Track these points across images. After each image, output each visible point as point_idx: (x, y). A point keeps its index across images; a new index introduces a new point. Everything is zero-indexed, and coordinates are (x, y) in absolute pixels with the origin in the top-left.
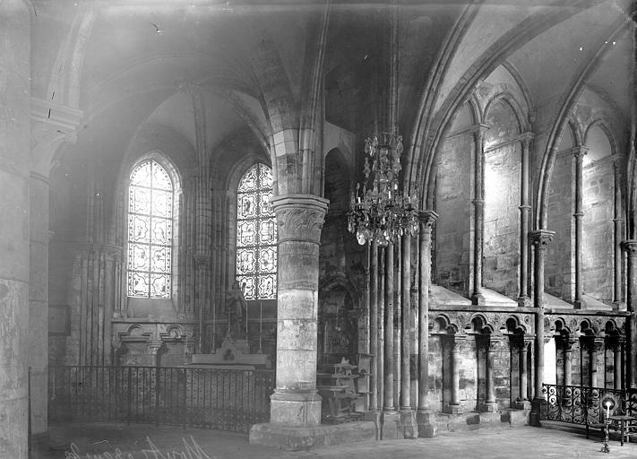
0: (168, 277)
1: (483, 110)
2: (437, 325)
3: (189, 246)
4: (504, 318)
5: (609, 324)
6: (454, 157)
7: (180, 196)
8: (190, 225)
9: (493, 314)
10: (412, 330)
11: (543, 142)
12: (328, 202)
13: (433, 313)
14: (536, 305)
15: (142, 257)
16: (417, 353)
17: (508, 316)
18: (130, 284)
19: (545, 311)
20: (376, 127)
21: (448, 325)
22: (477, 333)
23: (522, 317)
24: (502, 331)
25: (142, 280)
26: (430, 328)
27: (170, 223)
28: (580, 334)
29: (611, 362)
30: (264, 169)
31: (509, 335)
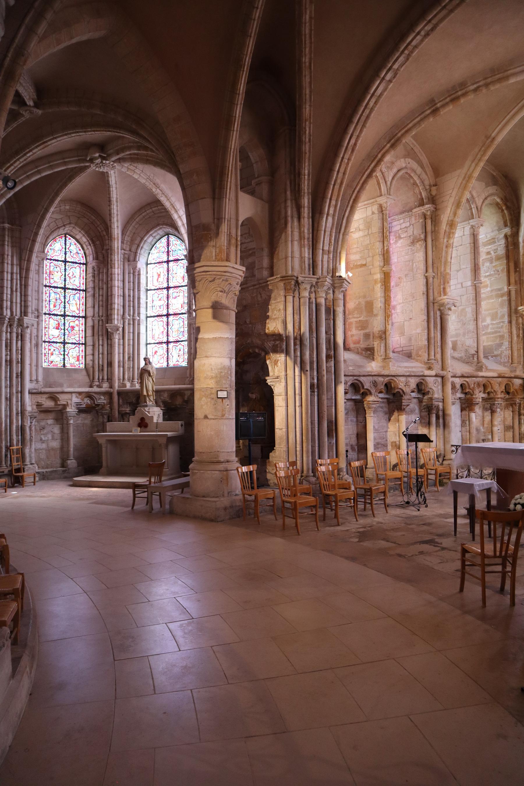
0: (82, 347)
1: (389, 183)
2: (351, 390)
3: (102, 316)
4: (413, 382)
5: (507, 386)
6: (361, 227)
7: (93, 268)
8: (103, 296)
9: (371, 378)
10: (65, 385)
11: (151, 238)
12: (244, 269)
13: (348, 379)
14: (443, 369)
15: (57, 328)
16: (334, 419)
17: (418, 380)
18: (45, 355)
19: (452, 375)
20: (7, 233)
21: (362, 391)
22: (419, 396)
23: (430, 380)
24: (412, 394)
25: (57, 352)
26: (346, 393)
27: (83, 294)
28: (482, 395)
29: (509, 422)
30: (172, 239)
31: (387, 398)
